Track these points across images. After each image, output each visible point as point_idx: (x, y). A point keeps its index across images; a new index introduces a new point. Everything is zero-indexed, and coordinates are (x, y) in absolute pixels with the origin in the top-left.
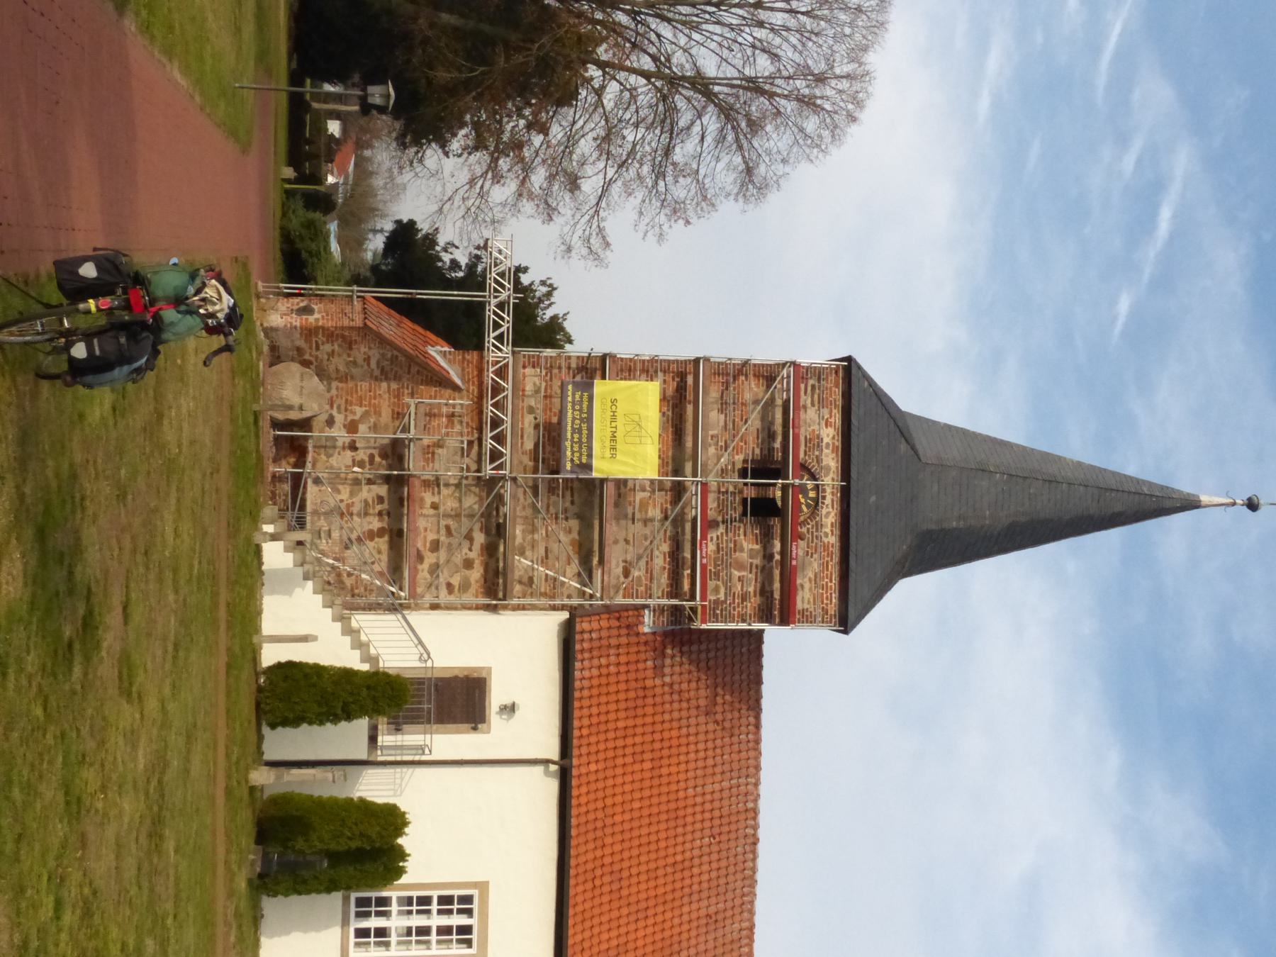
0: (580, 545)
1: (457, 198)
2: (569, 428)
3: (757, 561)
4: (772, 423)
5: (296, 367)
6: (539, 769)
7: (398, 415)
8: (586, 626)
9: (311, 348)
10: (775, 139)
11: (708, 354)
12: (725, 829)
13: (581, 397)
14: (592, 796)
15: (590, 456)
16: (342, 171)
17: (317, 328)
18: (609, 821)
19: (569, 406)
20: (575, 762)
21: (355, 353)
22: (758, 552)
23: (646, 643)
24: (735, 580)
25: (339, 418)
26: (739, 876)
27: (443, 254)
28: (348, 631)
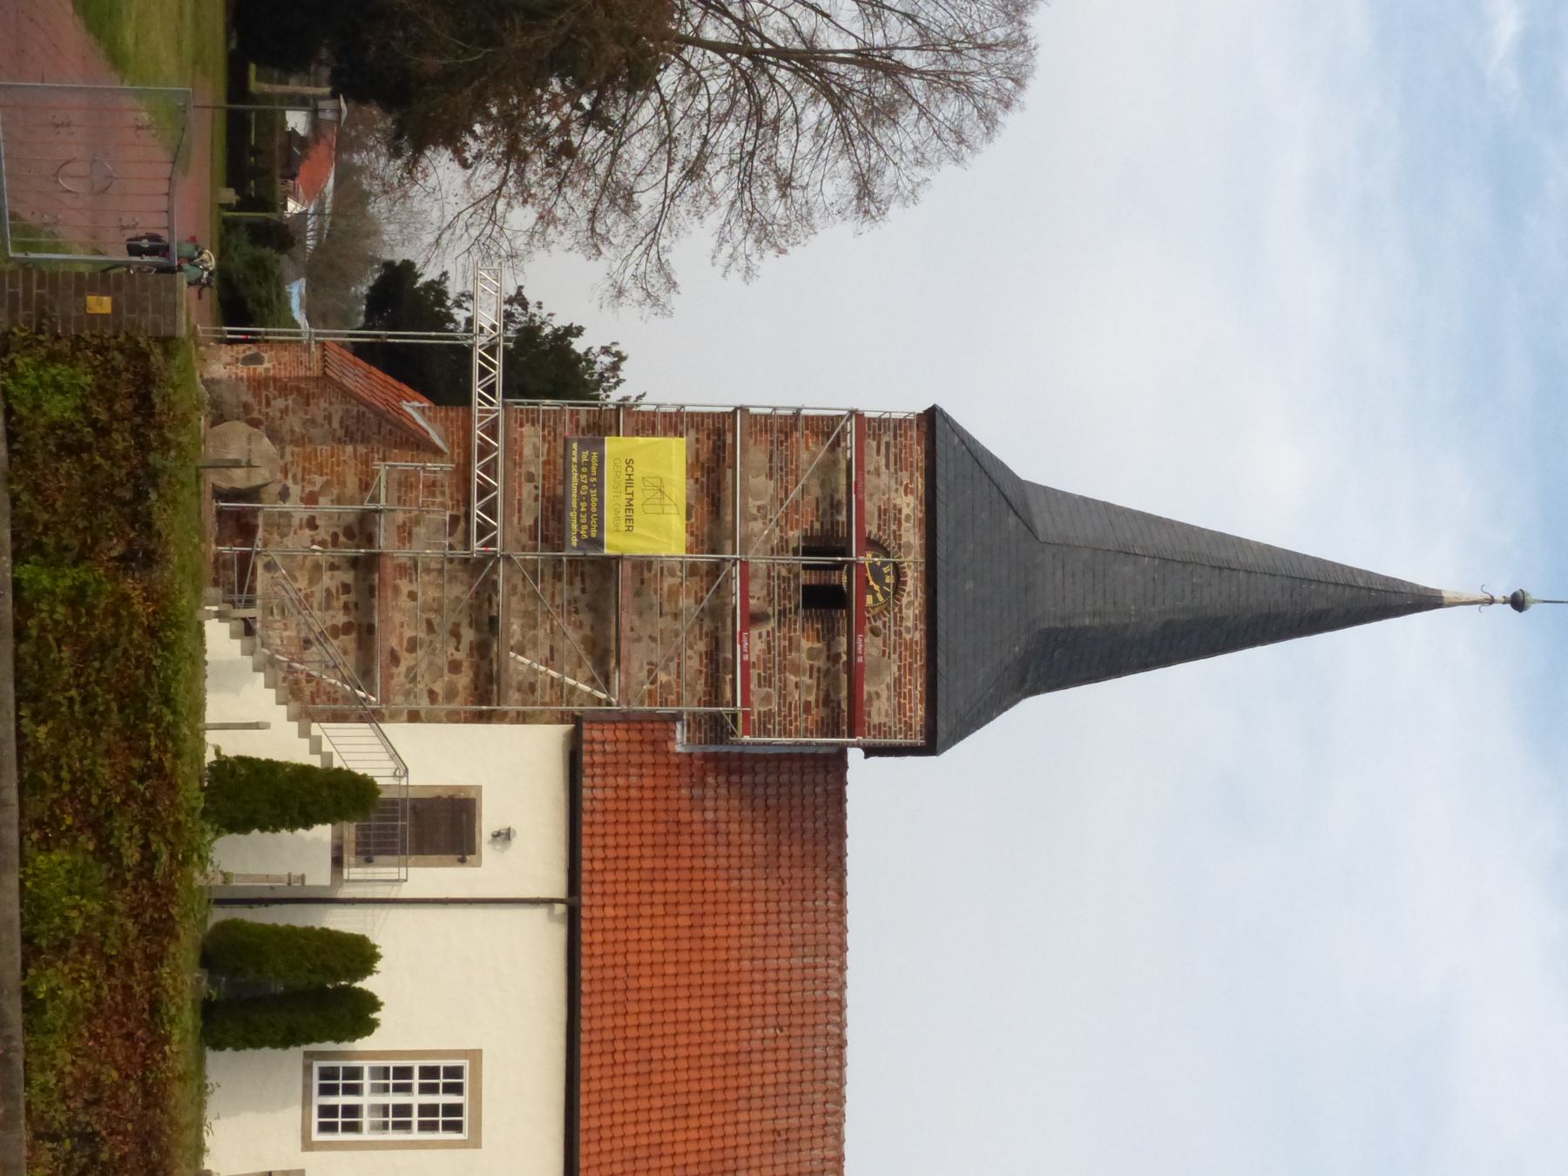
1: (461, 224)
2: (574, 495)
3: (821, 663)
4: (835, 490)
5: (241, 427)
6: (540, 913)
7: (365, 486)
8: (597, 734)
9: (260, 403)
10: (908, 132)
11: (745, 403)
12: (797, 1020)
13: (589, 457)
14: (609, 948)
15: (601, 528)
16: (315, 191)
17: (267, 379)
18: (633, 984)
19: (574, 468)
20: (585, 900)
21: (312, 409)
22: (819, 651)
23: (678, 766)
24: (791, 687)
25: (295, 490)
26: (819, 1086)
27: (455, 311)
28: (304, 733)
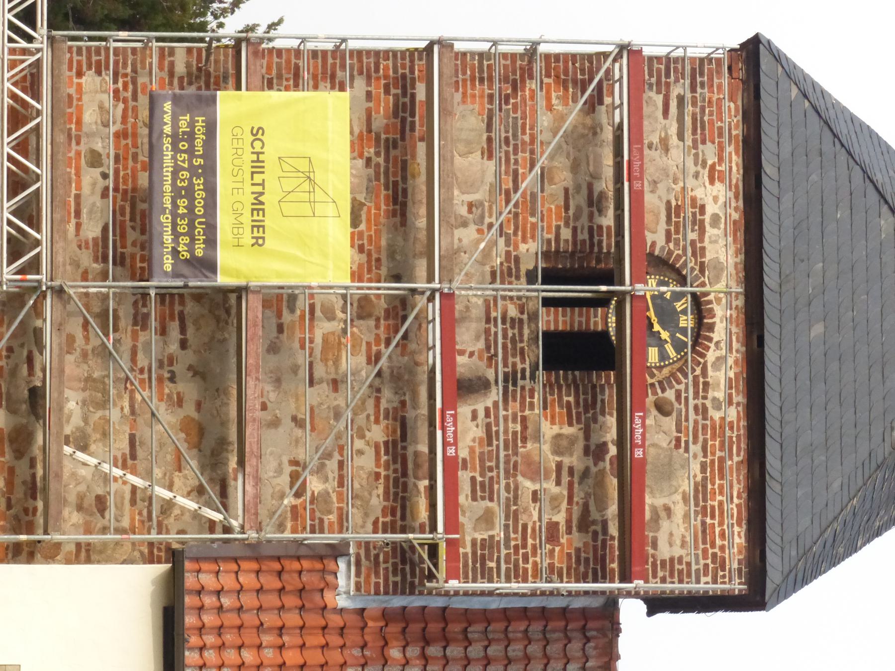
0: (201, 431)
3: (575, 460)
8: (207, 580)
13: (192, 124)
15: (211, 242)
19: (167, 143)
24: (526, 498)
